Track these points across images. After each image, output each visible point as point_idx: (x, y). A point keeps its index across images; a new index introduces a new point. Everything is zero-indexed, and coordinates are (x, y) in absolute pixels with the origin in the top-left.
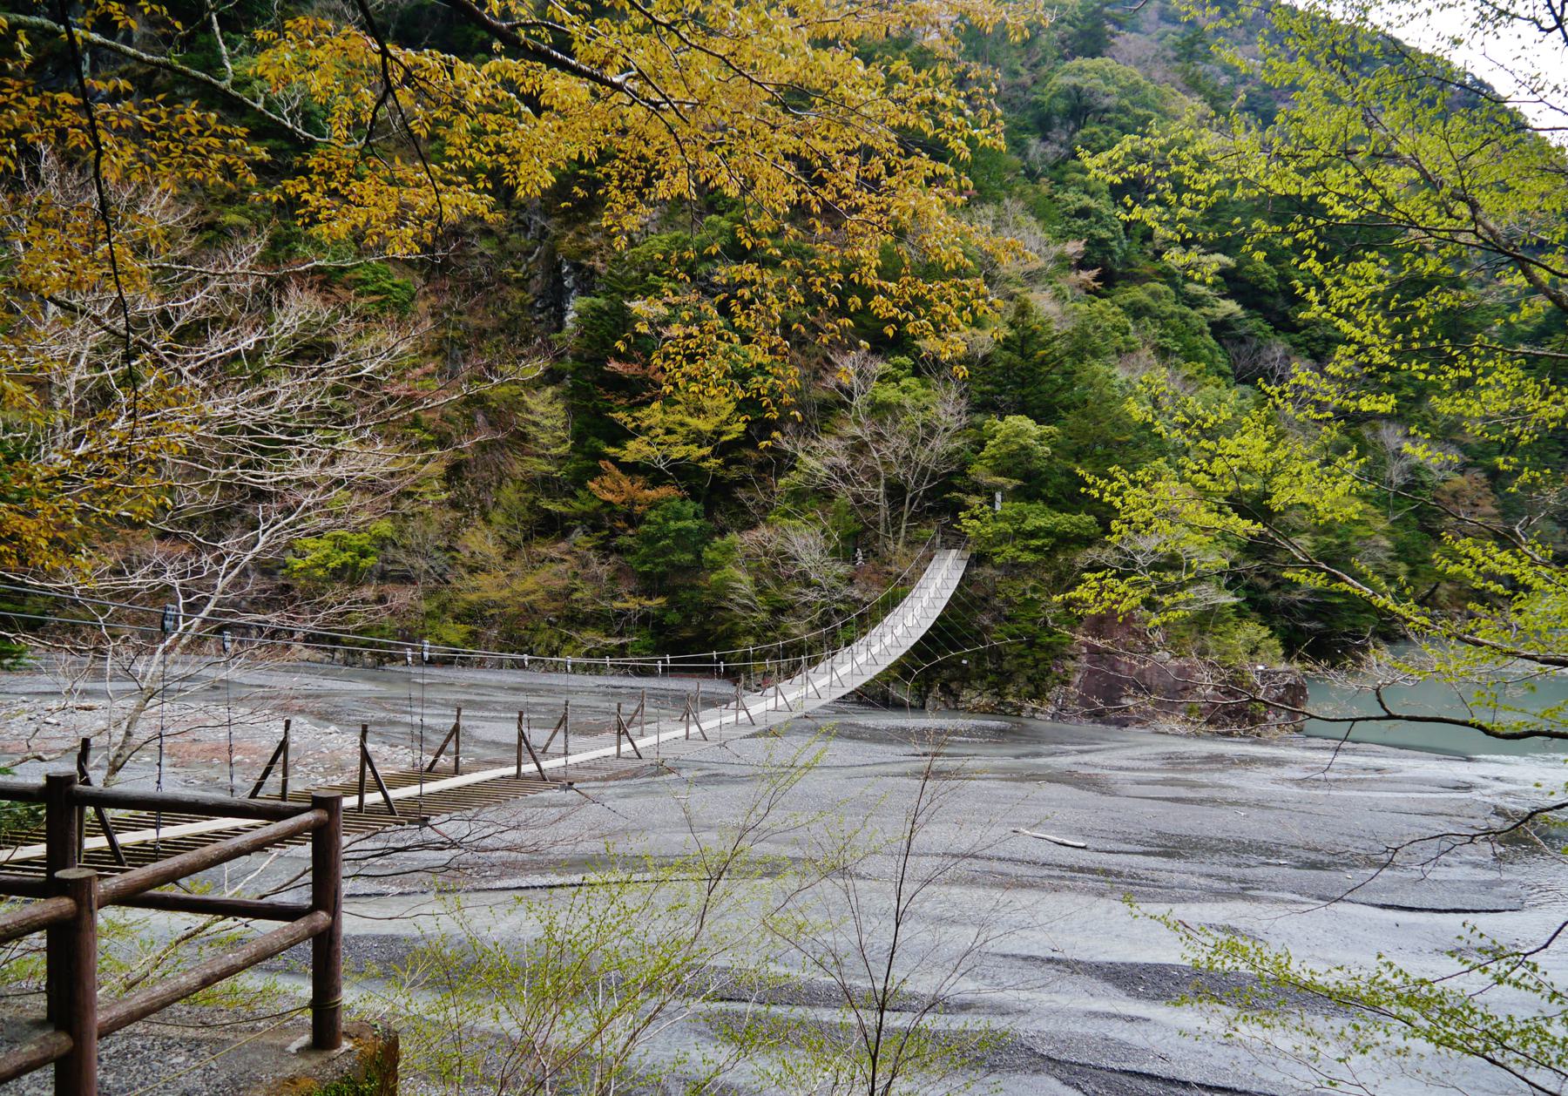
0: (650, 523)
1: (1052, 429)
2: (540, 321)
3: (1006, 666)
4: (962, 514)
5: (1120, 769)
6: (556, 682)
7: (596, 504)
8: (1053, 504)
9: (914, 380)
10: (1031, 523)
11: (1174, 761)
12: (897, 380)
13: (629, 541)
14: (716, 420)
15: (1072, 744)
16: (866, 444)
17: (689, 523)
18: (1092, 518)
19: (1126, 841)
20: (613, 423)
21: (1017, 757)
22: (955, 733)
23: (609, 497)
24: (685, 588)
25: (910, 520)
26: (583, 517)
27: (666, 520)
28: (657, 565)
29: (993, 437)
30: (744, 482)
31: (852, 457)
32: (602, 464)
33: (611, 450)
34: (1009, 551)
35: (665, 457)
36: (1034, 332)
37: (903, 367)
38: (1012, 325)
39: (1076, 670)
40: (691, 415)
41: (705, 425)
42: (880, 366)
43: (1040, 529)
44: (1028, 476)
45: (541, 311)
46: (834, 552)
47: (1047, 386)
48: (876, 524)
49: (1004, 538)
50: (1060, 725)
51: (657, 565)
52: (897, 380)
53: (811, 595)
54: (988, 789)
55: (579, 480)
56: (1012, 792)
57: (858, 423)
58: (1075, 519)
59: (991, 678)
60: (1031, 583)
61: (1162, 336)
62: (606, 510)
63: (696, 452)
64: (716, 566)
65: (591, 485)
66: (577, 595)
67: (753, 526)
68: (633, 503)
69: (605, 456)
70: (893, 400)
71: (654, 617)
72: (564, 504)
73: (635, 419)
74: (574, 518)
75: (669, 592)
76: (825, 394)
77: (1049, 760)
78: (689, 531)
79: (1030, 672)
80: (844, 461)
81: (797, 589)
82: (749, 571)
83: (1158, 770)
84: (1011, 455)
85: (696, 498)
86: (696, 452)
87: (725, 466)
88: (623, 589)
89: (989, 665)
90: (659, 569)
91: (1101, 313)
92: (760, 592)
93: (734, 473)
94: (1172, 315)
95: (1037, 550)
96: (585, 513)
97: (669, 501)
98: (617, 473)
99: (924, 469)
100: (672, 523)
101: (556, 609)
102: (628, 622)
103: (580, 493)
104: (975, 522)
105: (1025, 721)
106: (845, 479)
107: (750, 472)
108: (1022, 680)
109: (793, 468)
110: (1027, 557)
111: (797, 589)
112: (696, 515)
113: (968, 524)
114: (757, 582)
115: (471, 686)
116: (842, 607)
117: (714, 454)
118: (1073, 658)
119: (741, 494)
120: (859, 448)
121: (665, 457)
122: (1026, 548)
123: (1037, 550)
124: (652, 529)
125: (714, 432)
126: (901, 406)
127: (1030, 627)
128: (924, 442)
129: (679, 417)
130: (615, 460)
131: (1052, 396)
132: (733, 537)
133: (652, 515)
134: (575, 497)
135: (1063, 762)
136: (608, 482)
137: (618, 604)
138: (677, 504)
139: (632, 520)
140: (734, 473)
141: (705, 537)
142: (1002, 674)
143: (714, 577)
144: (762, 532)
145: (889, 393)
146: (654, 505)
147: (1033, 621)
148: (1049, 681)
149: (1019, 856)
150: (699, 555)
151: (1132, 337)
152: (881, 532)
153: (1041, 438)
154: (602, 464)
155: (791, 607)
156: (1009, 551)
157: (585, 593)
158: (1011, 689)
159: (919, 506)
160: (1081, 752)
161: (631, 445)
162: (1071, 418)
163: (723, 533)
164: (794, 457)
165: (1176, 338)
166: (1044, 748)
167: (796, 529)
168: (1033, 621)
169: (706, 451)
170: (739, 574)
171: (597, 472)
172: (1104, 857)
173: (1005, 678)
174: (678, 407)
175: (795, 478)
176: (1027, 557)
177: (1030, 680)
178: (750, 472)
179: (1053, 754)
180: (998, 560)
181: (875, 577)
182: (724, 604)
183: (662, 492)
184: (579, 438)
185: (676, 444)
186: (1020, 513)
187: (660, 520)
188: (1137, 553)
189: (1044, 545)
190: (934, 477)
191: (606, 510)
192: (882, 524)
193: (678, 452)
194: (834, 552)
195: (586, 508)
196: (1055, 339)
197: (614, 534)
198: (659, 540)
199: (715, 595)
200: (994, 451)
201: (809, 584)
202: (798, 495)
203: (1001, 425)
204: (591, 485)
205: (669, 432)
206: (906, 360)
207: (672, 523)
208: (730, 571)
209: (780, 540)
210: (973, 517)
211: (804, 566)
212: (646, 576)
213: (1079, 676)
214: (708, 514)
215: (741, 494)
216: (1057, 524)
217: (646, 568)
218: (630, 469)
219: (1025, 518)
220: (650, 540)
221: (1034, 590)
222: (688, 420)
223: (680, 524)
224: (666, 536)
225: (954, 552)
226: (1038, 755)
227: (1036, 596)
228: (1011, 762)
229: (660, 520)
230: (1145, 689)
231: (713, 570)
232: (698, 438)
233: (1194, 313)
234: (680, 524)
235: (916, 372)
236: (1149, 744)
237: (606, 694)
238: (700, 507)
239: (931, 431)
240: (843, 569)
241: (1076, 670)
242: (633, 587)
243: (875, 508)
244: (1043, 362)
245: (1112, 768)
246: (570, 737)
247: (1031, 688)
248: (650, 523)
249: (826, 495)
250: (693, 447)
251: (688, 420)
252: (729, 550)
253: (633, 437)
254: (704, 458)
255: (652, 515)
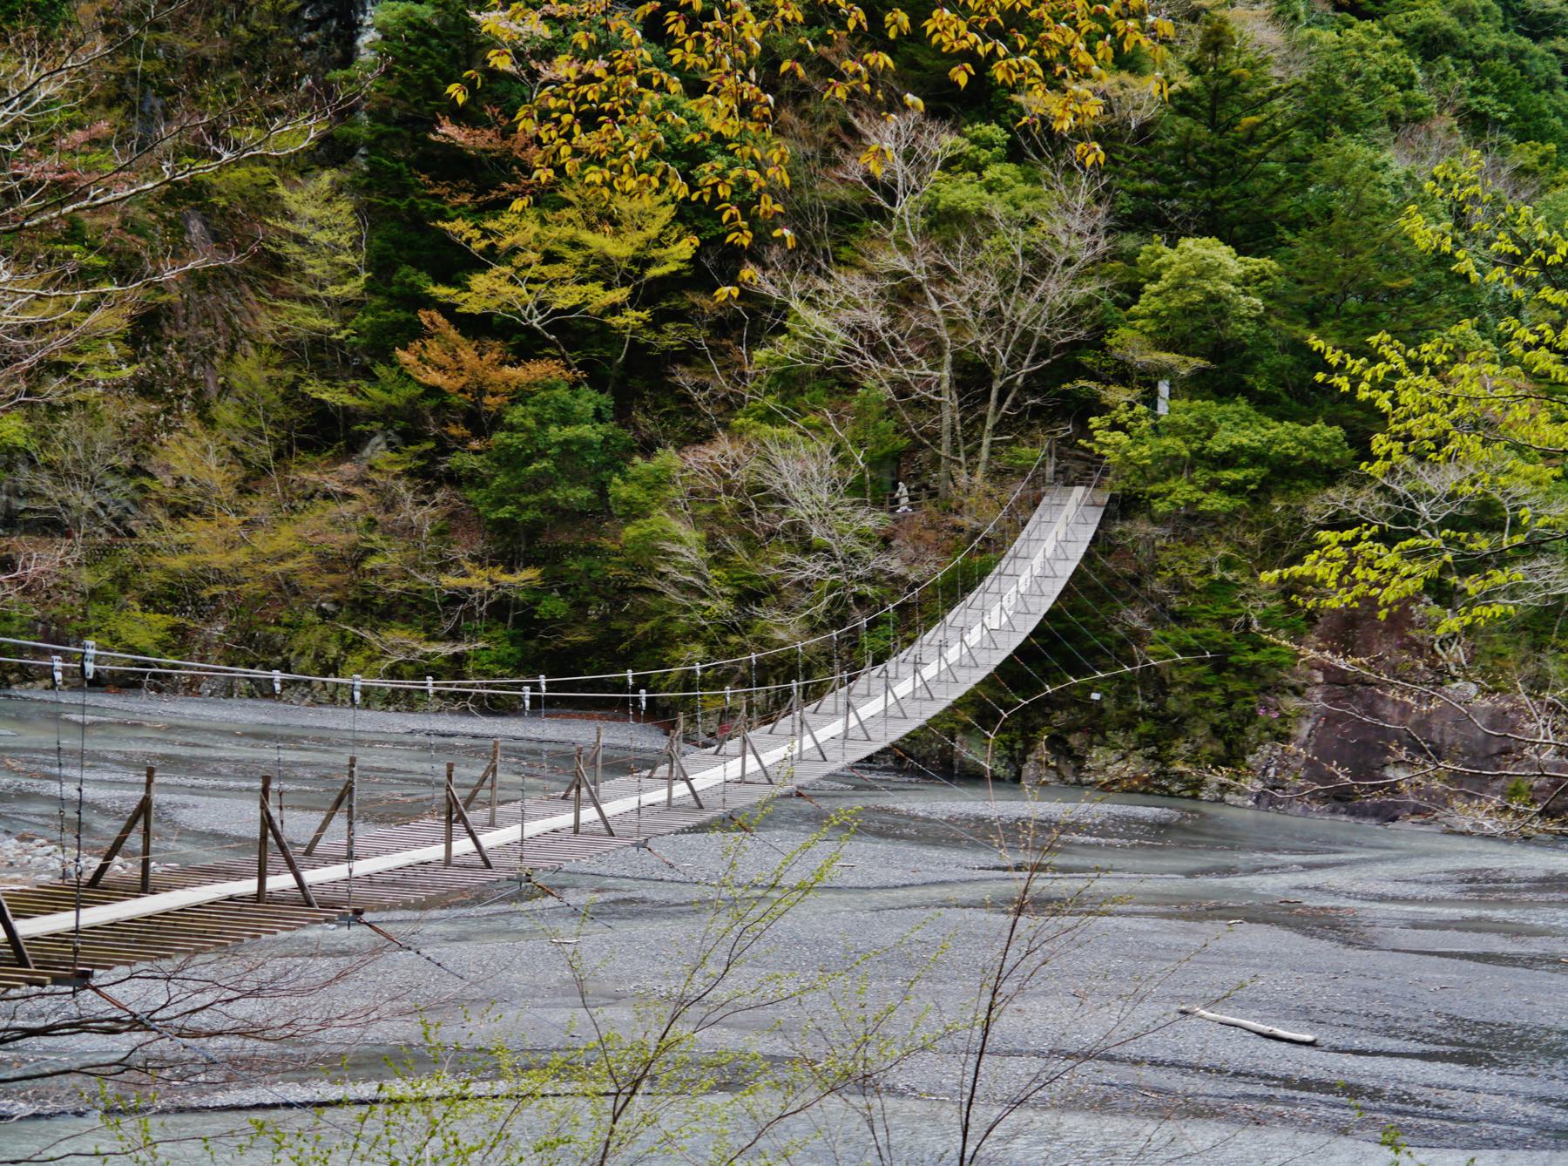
0: (512, 428)
1: (1266, 264)
2: (311, 46)
3: (1172, 705)
4: (1095, 421)
5: (1382, 898)
6: (332, 724)
7: (412, 391)
8: (1265, 404)
9: (1011, 168)
10: (1220, 443)
11: (1482, 885)
12: (978, 168)
13: (472, 462)
14: (637, 238)
15: (1293, 851)
16: (918, 287)
17: (585, 431)
18: (1337, 431)
19: (1389, 1032)
20: (445, 239)
21: (1190, 874)
22: (1076, 827)
23: (436, 378)
24: (576, 552)
25: (997, 430)
26: (387, 415)
27: (543, 423)
28: (524, 507)
29: (1155, 278)
30: (689, 355)
31: (890, 309)
32: (424, 316)
33: (441, 291)
34: (1182, 490)
35: (541, 305)
36: (1236, 81)
37: (989, 145)
38: (1195, 68)
39: (1301, 714)
40: (591, 227)
41: (619, 248)
42: (946, 142)
43: (1239, 450)
44: (1221, 351)
45: (313, 26)
46: (856, 488)
47: (1257, 184)
48: (935, 436)
49: (1173, 466)
50: (1270, 816)
51: (524, 507)
52: (978, 168)
53: (812, 568)
54: (1135, 933)
55: (382, 345)
56: (1180, 939)
57: (905, 248)
58: (1305, 432)
59: (1144, 727)
60: (1222, 551)
61: (1475, 92)
62: (431, 403)
63: (600, 297)
64: (634, 512)
65: (404, 356)
66: (374, 562)
67: (704, 437)
68: (481, 391)
69: (430, 302)
70: (969, 205)
71: (517, 605)
72: (352, 391)
73: (486, 234)
74: (370, 417)
75: (548, 559)
76: (842, 193)
77: (1252, 881)
78: (586, 445)
79: (1217, 717)
80: (876, 319)
81: (785, 556)
82: (697, 521)
83: (1451, 902)
84: (1189, 312)
85: (598, 383)
86: (600, 297)
87: (655, 325)
88: (460, 552)
89: (1140, 704)
90: (529, 515)
91: (1361, 48)
92: (717, 561)
93: (671, 337)
94: (1495, 53)
95: (1233, 489)
96: (390, 408)
97: (547, 387)
98: (453, 334)
99: (1027, 335)
100: (553, 429)
101: (333, 588)
102: (469, 614)
103: (381, 370)
104: (1119, 436)
105: (1205, 808)
106: (878, 351)
107: (701, 336)
108: (1201, 732)
109: (782, 330)
110: (1216, 502)
111: (785, 556)
112: (598, 416)
113: (1106, 439)
114: (711, 542)
115: (171, 728)
116: (869, 590)
117: (634, 302)
118: (1297, 692)
119: (684, 377)
120: (904, 294)
121: (541, 305)
122: (1214, 485)
123: (1233, 489)
124: (516, 440)
125: (635, 261)
126: (984, 217)
127: (1218, 634)
128: (1027, 284)
129: (568, 231)
130: (448, 310)
131: (1268, 203)
132: (667, 457)
133: (515, 415)
134: (373, 379)
135: (1271, 885)
136: (434, 351)
137: (450, 581)
138: (563, 394)
139: (480, 423)
140: (671, 337)
141: (616, 458)
142: (1164, 720)
143: (630, 531)
144: (722, 449)
145: (963, 193)
146: (519, 396)
147: (1225, 622)
148: (1252, 733)
149: (1192, 1058)
150: (602, 490)
151: (1419, 93)
152: (944, 451)
153: (1246, 280)
154: (424, 316)
155: (774, 589)
156: (1182, 490)
157: (389, 558)
158: (1182, 747)
159: (1016, 404)
160: (1309, 867)
161: (479, 282)
162: (1302, 245)
163: (648, 448)
164: (783, 309)
165: (1503, 96)
166: (1240, 859)
167: (784, 444)
168: (1225, 622)
169: (620, 294)
170: (678, 527)
171: (416, 332)
172: (1349, 1061)
173: (1173, 727)
174: (569, 213)
175: (785, 349)
176: (1216, 502)
177: (1217, 732)
178: (701, 336)
179: (1257, 870)
180: (1161, 507)
181: (930, 535)
182: (648, 582)
183: (536, 370)
184: (382, 267)
185: (562, 281)
186: (1202, 420)
187: (530, 423)
188: (1420, 498)
189: (1247, 481)
190: (1044, 350)
191: (431, 403)
192: (946, 438)
193: (566, 297)
194: (856, 488)
195: (393, 400)
196: (1274, 94)
197: (444, 449)
198: (529, 460)
199: (632, 565)
200: (1157, 303)
201: (807, 548)
202: (789, 381)
203: (1170, 255)
204: (404, 356)
205: (550, 258)
206: (994, 131)
207: (553, 429)
208: (660, 519)
209: (755, 464)
210: (1115, 426)
211: (799, 512)
212: (503, 526)
213: (1307, 726)
214: (622, 415)
215: (684, 377)
216: (1272, 441)
217: (504, 513)
218: (477, 327)
219: (1213, 429)
220: (511, 460)
221: (1227, 564)
222: (586, 236)
223: (569, 432)
224: (542, 454)
225: (1079, 491)
226: (1229, 871)
227: (1230, 576)
228: (1181, 884)
229: (530, 423)
230: (1424, 747)
231: (629, 518)
232: (603, 271)
233: (1538, 49)
234: (569, 432)
235: (1014, 153)
236: (1440, 854)
237: (426, 748)
238: (606, 400)
239: (1041, 265)
240: (871, 520)
241: (1301, 714)
242: (479, 547)
243: (932, 407)
244: (1252, 138)
245: (1367, 897)
246: (359, 826)
247: (1219, 747)
248: (512, 428)
249: (842, 381)
250: (595, 288)
251: (586, 236)
252: (659, 482)
253: (483, 267)
254: (615, 309)
255: (515, 415)
